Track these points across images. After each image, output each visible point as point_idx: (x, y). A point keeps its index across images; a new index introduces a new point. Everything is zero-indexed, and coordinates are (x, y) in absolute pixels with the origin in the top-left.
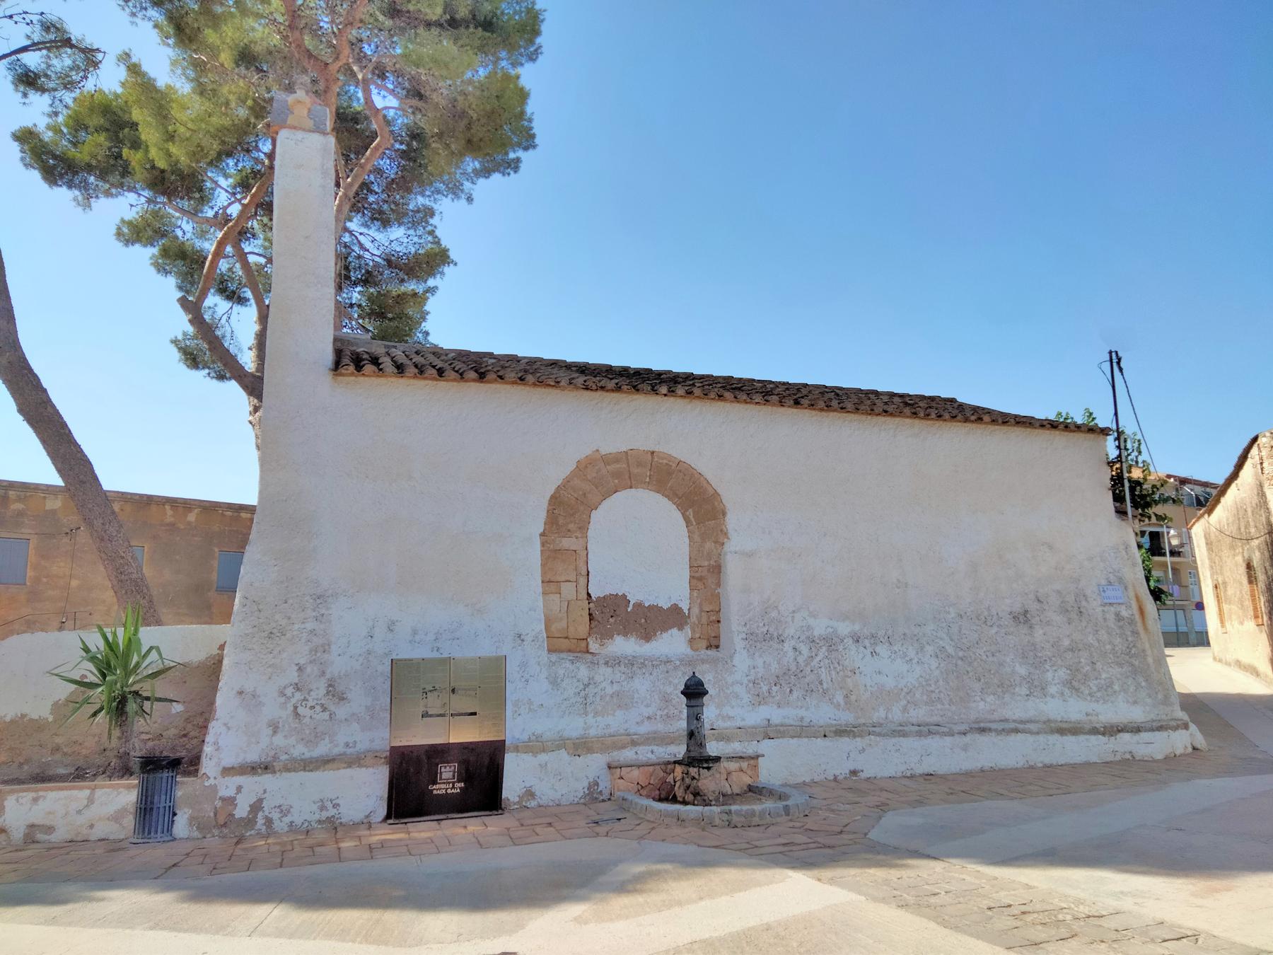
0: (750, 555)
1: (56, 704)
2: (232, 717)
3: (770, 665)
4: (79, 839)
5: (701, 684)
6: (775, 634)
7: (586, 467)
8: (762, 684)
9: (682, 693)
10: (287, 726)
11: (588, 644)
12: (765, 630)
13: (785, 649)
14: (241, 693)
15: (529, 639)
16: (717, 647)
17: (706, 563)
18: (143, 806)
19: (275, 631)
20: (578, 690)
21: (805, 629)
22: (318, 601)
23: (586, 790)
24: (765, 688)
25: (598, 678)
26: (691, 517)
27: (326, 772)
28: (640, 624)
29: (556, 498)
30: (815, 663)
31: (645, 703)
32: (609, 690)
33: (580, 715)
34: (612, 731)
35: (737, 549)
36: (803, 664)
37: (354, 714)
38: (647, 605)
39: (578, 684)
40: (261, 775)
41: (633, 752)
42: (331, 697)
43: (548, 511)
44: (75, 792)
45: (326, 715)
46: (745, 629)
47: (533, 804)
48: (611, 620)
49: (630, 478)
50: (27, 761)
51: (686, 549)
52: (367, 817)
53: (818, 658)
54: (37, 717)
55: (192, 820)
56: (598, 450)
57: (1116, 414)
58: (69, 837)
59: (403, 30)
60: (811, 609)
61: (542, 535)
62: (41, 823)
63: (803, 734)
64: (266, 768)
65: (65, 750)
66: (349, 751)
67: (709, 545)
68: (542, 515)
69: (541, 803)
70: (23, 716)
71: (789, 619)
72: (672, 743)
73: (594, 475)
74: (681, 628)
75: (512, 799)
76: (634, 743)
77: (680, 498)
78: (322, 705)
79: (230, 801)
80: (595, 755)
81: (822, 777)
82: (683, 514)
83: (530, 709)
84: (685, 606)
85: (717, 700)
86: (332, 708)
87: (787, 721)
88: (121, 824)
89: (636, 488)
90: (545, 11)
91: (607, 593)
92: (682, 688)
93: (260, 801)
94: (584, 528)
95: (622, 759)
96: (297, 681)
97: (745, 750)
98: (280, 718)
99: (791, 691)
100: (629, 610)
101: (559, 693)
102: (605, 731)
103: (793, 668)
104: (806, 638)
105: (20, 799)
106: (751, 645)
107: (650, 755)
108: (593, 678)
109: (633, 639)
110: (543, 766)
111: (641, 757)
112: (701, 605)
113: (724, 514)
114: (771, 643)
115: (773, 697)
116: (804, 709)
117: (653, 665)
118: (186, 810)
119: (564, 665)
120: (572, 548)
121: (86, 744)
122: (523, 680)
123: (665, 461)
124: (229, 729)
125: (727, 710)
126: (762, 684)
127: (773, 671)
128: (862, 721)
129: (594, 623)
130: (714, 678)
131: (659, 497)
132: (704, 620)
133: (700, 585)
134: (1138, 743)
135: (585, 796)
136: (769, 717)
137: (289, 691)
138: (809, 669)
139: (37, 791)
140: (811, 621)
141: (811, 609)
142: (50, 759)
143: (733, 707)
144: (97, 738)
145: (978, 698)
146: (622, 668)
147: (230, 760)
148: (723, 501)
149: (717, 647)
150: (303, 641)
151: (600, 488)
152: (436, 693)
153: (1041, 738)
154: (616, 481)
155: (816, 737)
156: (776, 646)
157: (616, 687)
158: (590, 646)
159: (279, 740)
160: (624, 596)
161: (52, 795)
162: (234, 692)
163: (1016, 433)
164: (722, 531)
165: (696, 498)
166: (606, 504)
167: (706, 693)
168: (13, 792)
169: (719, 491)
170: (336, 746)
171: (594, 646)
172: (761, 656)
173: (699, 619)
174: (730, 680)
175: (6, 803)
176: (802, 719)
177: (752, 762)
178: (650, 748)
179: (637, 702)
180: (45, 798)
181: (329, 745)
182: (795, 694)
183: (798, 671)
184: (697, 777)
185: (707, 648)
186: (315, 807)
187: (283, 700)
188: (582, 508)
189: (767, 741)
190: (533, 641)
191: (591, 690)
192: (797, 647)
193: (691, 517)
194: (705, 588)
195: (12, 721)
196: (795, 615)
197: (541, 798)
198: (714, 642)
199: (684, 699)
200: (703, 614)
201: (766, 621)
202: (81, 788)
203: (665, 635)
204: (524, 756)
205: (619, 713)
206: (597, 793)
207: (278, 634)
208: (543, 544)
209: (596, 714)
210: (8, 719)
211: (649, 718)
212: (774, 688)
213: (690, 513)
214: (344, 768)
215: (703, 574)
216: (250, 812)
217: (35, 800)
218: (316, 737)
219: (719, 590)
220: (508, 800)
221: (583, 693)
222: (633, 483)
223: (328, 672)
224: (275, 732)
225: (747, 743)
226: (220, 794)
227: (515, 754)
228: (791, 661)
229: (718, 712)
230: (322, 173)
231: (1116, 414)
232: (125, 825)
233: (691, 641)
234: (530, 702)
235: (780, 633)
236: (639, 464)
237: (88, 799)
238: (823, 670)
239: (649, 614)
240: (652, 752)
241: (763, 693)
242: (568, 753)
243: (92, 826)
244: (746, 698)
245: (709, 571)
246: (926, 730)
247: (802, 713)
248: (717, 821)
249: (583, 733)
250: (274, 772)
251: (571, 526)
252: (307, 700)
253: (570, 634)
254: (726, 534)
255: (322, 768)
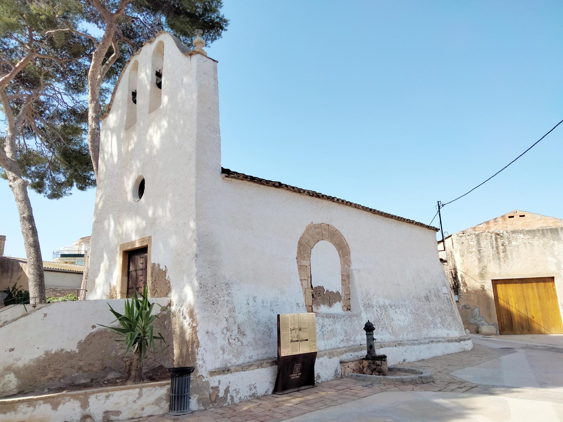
1: (80, 343)
2: (206, 345)
4: (137, 417)
9: (364, 329)
10: (228, 349)
14: (207, 333)
16: (350, 310)
18: (176, 395)
19: (214, 301)
20: (320, 329)
22: (227, 286)
25: (325, 324)
27: (250, 371)
32: (329, 329)
37: (249, 342)
40: (227, 374)
42: (240, 334)
44: (131, 391)
45: (239, 343)
49: (322, 235)
50: (64, 377)
52: (266, 392)
54: (70, 351)
55: (199, 401)
57: (441, 222)
58: (130, 416)
59: (157, 12)
62: (112, 410)
64: (228, 370)
65: (84, 369)
66: (251, 360)
68: (296, 249)
70: (62, 350)
71: (373, 298)
72: (356, 351)
78: (237, 338)
79: (216, 389)
86: (241, 339)
88: (159, 406)
90: (230, 20)
93: (228, 387)
94: (309, 256)
96: (226, 326)
98: (224, 345)
100: (325, 293)
105: (98, 397)
118: (195, 395)
121: (96, 365)
123: (332, 229)
124: (206, 351)
128: (397, 339)
134: (465, 345)
137: (225, 331)
139: (108, 391)
142: (77, 374)
144: (101, 362)
145: (423, 329)
147: (210, 368)
150: (226, 306)
152: (295, 331)
153: (445, 344)
159: (226, 356)
161: (117, 393)
162: (205, 332)
163: (405, 225)
167: (374, 329)
168: (93, 393)
170: (246, 358)
175: (90, 400)
180: (113, 395)
181: (244, 358)
184: (380, 365)
186: (248, 389)
187: (223, 336)
189: (381, 349)
191: (324, 329)
195: (56, 354)
198: (349, 308)
199: (365, 332)
202: (134, 388)
207: (216, 303)
210: (53, 352)
213: (340, 251)
214: (256, 369)
216: (224, 394)
217: (107, 397)
218: (239, 354)
223: (237, 321)
224: (224, 352)
226: (211, 385)
230: (214, 79)
231: (441, 222)
232: (162, 407)
237: (139, 394)
243: (143, 409)
246: (413, 342)
248: (418, 382)
250: (231, 372)
251: (305, 255)
252: (232, 336)
254: (350, 262)
255: (248, 369)
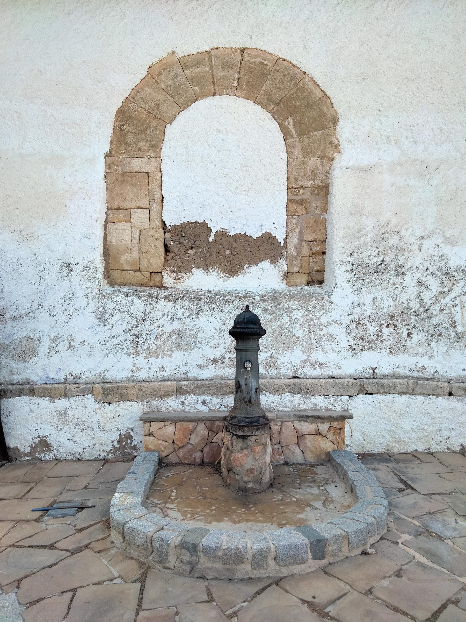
0: (366, 170)
3: (382, 302)
5: (255, 320)
6: (393, 265)
7: (160, 74)
8: (369, 325)
9: (231, 333)
11: (162, 277)
12: (379, 260)
13: (405, 284)
15: (78, 269)
17: (309, 184)
20: (130, 327)
21: (436, 258)
23: (116, 443)
24: (372, 330)
25: (155, 314)
26: (291, 128)
28: (225, 257)
29: (124, 112)
30: (447, 300)
31: (211, 344)
32: (168, 328)
33: (129, 355)
34: (166, 374)
35: (350, 164)
36: (429, 302)
38: (232, 234)
39: (130, 320)
41: (178, 402)
43: (114, 128)
46: (351, 259)
47: (48, 456)
48: (191, 252)
49: (214, 84)
51: (284, 167)
53: (452, 295)
56: (174, 52)
60: (447, 235)
61: (107, 156)
63: (418, 390)
67: (313, 161)
69: (58, 455)
71: (415, 247)
73: (170, 82)
74: (274, 260)
75: (22, 450)
76: (181, 391)
77: (276, 105)
80: (129, 403)
81: (443, 447)
82: (280, 125)
83: (70, 346)
84: (280, 236)
85: (304, 343)
87: (401, 372)
89: (220, 95)
91: (185, 220)
92: (231, 324)
95: (163, 409)
97: (330, 407)
99: (409, 335)
101: (106, 328)
102: (159, 374)
103: (415, 305)
104: (438, 270)
106: (357, 279)
107: (200, 406)
108: (149, 313)
109: (215, 273)
110: (63, 413)
111: (188, 408)
112: (301, 233)
113: (335, 121)
114: (386, 275)
115: (384, 341)
116: (426, 357)
117: (225, 301)
119: (115, 299)
120: (143, 170)
122: (66, 313)
123: (258, 60)
125: (318, 355)
126: (369, 325)
127: (385, 310)
129: (170, 255)
130: (304, 316)
131: (250, 105)
132: (305, 251)
133: (300, 210)
135: (114, 450)
136: (374, 366)
138: (437, 307)
140: (446, 250)
141: (447, 235)
143: (325, 352)
146: (186, 303)
148: (334, 105)
149: (321, 282)
151: (176, 98)
154: (196, 88)
155: (437, 395)
156: (393, 279)
157: (177, 324)
158: (165, 280)
160: (205, 224)
164: (331, 143)
165: (298, 104)
166: (183, 116)
169: (328, 92)
171: (168, 280)
172: (369, 291)
173: (298, 249)
174: (324, 319)
176: (423, 369)
177: (335, 424)
178: (202, 398)
179: (200, 342)
182: (415, 338)
183: (422, 310)
185: (308, 284)
188: (154, 123)
189: (362, 397)
190: (83, 271)
191: (145, 327)
192: (423, 280)
193: (291, 128)
194: (307, 213)
196: (424, 242)
197: (57, 450)
198: (317, 277)
200: (304, 244)
201: (381, 249)
203: (254, 269)
204: (40, 400)
205: (177, 354)
206: (131, 448)
208: (109, 166)
209: (149, 354)
211: (215, 361)
212: (386, 331)
215: (305, 197)
219: (325, 216)
220: (18, 450)
221: (135, 331)
222: (217, 88)
225: (333, 398)
227: (29, 398)
228: (412, 297)
229: (305, 357)
233: (287, 275)
234: (71, 339)
235: (400, 263)
236: (225, 65)
238: (458, 309)
239: (234, 245)
240: (204, 403)
241: (369, 336)
242: (96, 400)
244: (345, 341)
245: (312, 193)
247: (424, 361)
249: (130, 375)
251: (142, 145)
253: (141, 267)
